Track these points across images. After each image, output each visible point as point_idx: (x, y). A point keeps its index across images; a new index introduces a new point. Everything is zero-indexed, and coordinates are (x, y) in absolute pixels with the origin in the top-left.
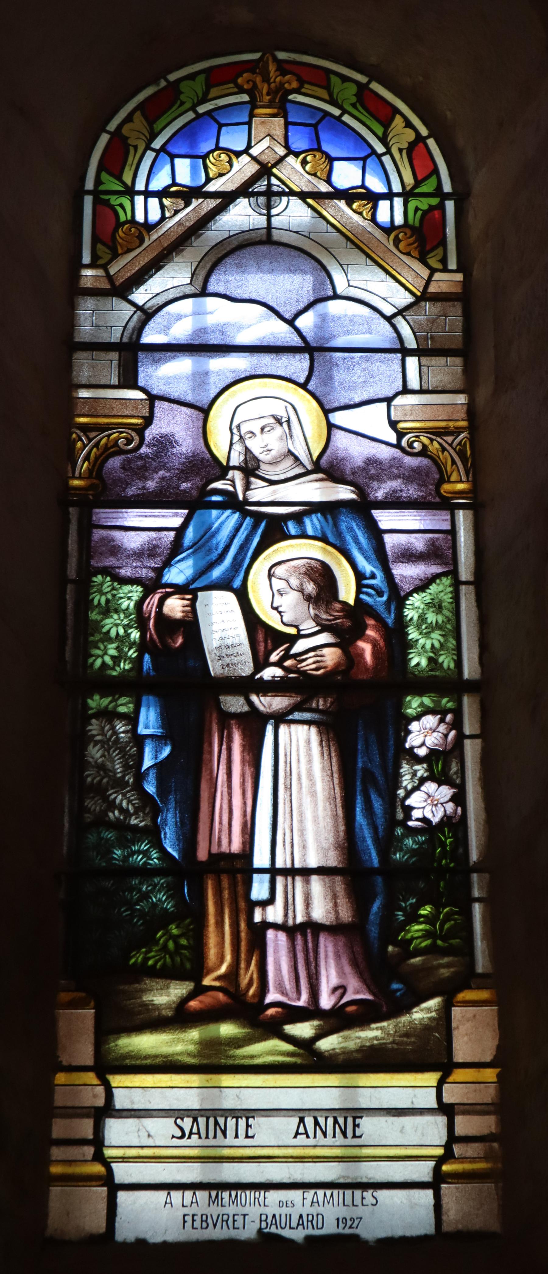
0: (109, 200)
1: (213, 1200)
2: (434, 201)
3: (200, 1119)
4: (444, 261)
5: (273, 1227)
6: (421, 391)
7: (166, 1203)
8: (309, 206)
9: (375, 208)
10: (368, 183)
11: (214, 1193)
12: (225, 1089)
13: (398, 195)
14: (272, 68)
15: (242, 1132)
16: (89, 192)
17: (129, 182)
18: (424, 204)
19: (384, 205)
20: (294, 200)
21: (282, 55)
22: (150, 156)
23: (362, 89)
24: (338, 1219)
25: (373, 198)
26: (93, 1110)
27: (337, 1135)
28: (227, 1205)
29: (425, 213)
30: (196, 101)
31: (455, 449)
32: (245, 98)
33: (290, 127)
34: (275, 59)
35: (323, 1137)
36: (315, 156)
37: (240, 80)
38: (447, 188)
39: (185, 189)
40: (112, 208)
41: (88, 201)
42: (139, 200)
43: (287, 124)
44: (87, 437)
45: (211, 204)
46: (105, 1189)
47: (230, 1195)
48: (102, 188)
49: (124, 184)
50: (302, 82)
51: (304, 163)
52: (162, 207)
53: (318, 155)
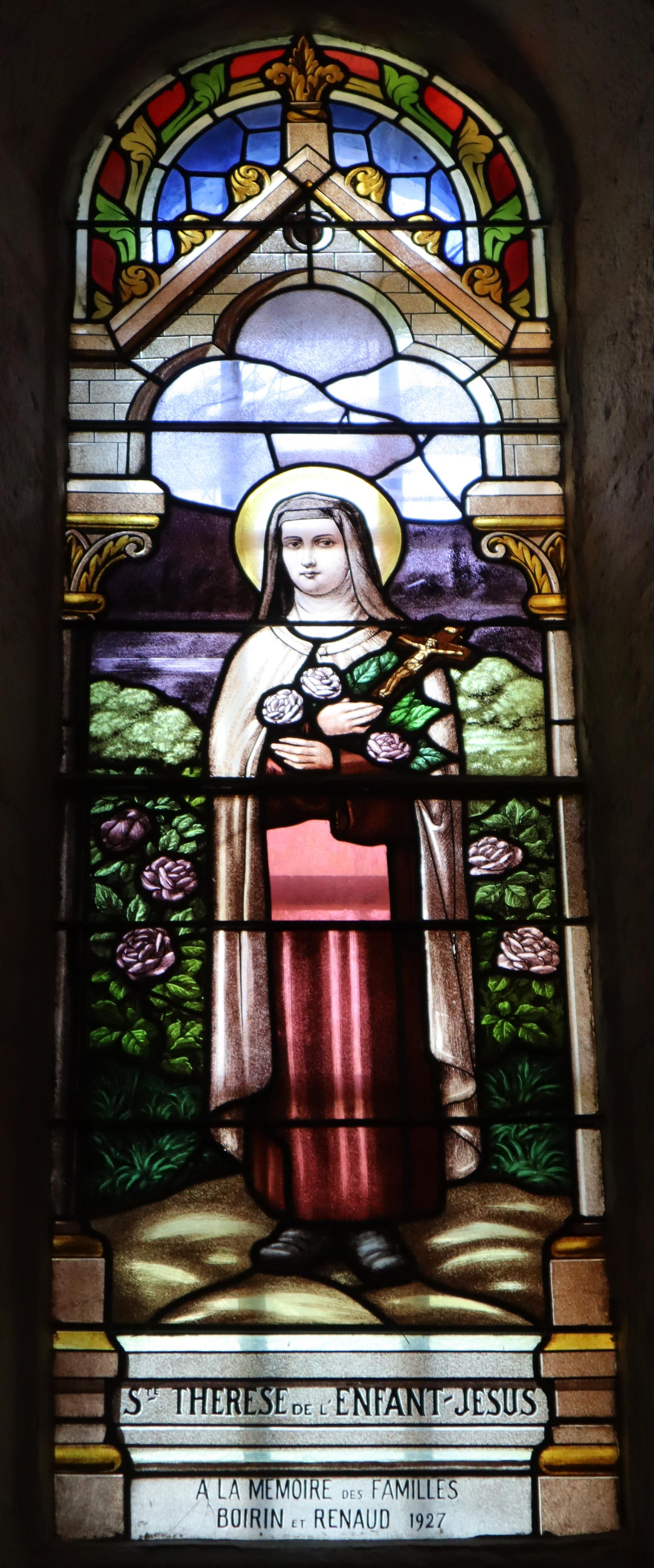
0: (108, 234)
1: (256, 1488)
2: (518, 230)
3: (400, 1391)
4: (531, 307)
5: (359, 1526)
6: (505, 478)
7: (199, 1493)
8: (360, 238)
9: (442, 242)
10: (433, 209)
11: (256, 1482)
12: (435, 1355)
13: (472, 224)
14: (308, 54)
15: (208, 1408)
16: (83, 225)
17: (133, 209)
18: (505, 234)
19: (454, 238)
20: (342, 233)
21: (322, 40)
22: (157, 175)
23: (424, 84)
24: (412, 1515)
25: (441, 227)
26: (103, 1382)
27: (412, 1413)
28: (274, 1496)
29: (507, 245)
30: (212, 101)
31: (546, 554)
32: (274, 95)
33: (336, 136)
34: (313, 45)
35: (364, 1413)
36: (366, 173)
37: (268, 73)
38: (534, 213)
39: (204, 219)
40: (114, 244)
41: (82, 236)
42: (146, 233)
43: (331, 131)
44: (88, 541)
45: (238, 236)
46: (121, 1476)
47: (278, 1484)
48: (98, 218)
49: (127, 212)
50: (348, 74)
51: (354, 183)
52: (177, 242)
53: (370, 171)
